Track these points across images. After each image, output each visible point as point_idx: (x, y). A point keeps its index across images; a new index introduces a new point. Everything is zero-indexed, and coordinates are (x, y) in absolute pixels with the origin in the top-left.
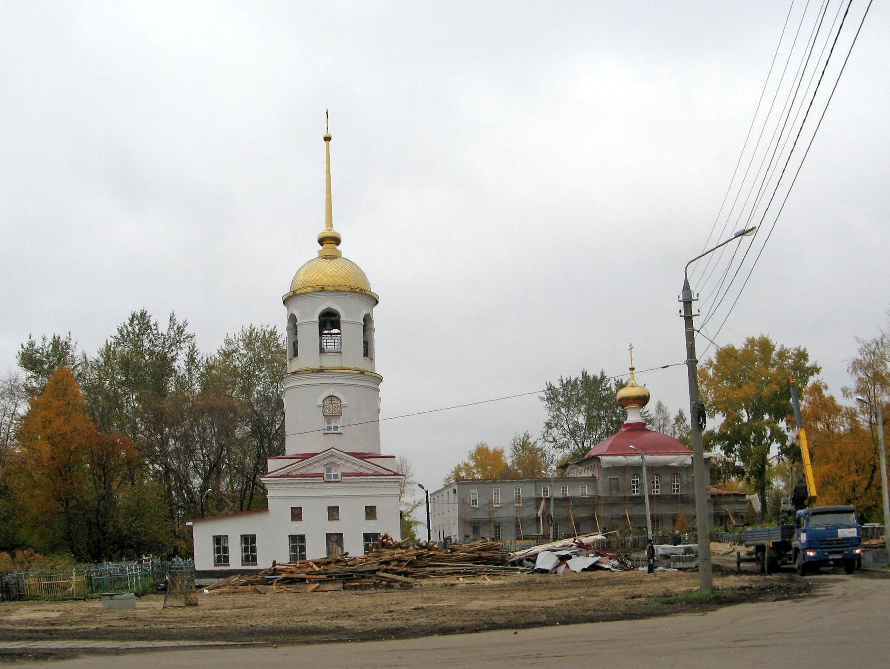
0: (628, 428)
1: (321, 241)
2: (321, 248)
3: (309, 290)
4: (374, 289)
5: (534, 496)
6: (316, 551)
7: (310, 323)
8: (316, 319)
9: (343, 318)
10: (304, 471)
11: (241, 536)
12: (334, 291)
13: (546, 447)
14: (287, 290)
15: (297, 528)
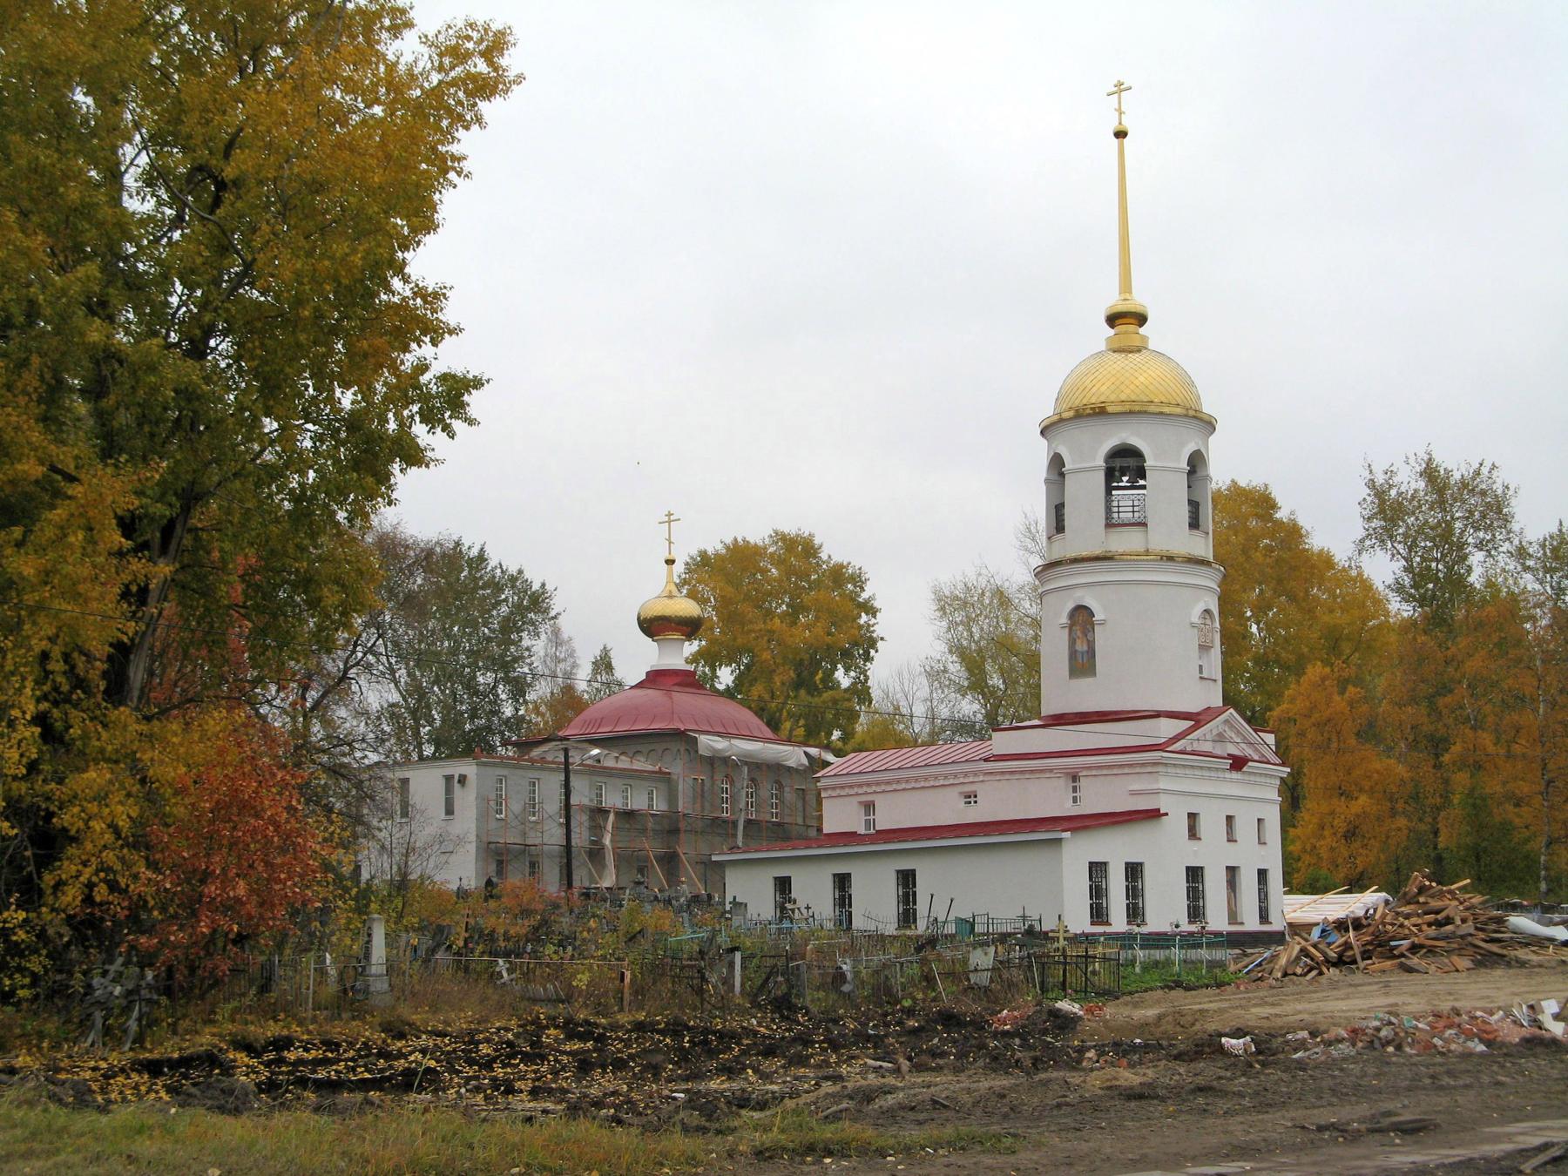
0: (678, 680)
1: (1113, 319)
2: (1112, 332)
3: (1178, 410)
4: (1208, 408)
8: (1100, 462)
9: (1149, 463)
10: (1189, 749)
11: (1188, 868)
12: (1186, 416)
13: (75, 732)
14: (1047, 411)
15: (1194, 854)
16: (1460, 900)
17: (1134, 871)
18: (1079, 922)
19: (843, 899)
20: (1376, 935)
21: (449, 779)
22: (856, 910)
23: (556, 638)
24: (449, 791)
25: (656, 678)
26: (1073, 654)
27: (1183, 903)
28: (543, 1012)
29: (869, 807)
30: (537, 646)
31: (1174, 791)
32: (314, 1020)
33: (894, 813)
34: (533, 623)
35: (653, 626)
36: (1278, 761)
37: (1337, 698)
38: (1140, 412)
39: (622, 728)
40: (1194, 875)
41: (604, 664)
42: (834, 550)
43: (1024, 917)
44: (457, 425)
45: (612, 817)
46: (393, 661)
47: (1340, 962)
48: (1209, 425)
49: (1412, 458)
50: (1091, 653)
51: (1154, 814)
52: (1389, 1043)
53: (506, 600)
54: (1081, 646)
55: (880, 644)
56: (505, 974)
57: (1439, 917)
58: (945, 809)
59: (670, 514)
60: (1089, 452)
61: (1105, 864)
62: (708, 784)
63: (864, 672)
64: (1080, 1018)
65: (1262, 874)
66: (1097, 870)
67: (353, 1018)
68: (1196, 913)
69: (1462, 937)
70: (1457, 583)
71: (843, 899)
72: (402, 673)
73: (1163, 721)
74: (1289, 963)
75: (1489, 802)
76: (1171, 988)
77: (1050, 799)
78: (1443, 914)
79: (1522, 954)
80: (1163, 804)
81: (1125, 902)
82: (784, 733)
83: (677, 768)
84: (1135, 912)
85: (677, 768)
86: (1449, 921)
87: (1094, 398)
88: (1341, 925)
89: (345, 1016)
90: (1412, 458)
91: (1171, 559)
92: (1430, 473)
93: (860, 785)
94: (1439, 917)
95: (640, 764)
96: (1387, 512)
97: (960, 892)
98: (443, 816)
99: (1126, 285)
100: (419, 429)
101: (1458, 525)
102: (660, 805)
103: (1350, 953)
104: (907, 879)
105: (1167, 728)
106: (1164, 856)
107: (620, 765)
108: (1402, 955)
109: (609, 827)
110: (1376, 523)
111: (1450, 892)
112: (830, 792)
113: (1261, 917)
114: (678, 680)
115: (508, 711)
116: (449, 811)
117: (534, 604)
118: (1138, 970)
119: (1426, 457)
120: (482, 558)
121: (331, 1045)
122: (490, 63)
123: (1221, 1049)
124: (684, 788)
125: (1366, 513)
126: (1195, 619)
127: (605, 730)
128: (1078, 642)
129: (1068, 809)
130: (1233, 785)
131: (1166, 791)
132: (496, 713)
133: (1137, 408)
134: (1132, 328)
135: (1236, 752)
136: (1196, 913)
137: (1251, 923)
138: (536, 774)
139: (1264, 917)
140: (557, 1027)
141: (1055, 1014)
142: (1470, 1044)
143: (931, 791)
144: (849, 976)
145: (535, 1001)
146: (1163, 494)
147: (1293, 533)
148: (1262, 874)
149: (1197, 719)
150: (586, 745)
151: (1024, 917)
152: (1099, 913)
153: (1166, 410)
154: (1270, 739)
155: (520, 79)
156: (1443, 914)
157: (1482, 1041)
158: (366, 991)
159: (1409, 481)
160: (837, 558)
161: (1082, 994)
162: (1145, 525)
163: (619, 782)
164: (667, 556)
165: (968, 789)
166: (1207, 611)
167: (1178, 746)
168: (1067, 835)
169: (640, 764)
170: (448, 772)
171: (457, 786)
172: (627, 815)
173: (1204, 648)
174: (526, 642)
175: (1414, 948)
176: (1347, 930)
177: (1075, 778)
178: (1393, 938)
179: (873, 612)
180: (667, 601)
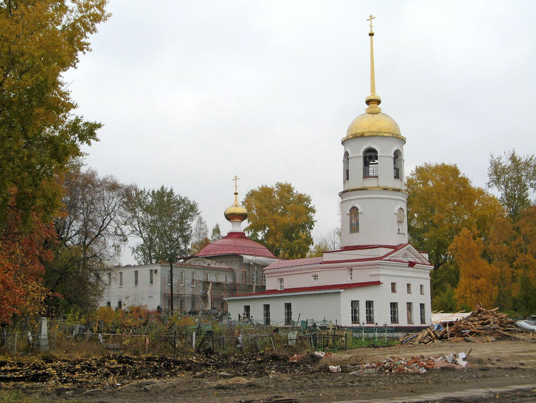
1: (368, 102)
2: (368, 107)
3: (390, 135)
4: (403, 134)
5: (202, 279)
6: (382, 318)
7: (388, 157)
8: (361, 154)
9: (379, 154)
10: (392, 259)
11: (367, 301)
14: (344, 135)
16: (493, 317)
17: (369, 304)
18: (346, 321)
19: (267, 314)
20: (456, 328)
21: (151, 271)
22: (272, 317)
23: (200, 221)
24: (151, 275)
25: (231, 235)
26: (351, 225)
27: (389, 316)
28: (112, 353)
29: (281, 280)
30: (193, 224)
31: (386, 274)
32: (16, 355)
33: (290, 283)
34: (191, 216)
35: (230, 217)
36: (429, 264)
37: (472, 242)
38: (375, 136)
39: (217, 253)
40: (394, 305)
41: (217, 230)
42: (299, 189)
43: (325, 321)
44: (92, 141)
45: (211, 284)
46: (142, 229)
47: (441, 338)
48: (403, 141)
49: (507, 152)
50: (357, 224)
51: (378, 283)
52: (387, 368)
53: (181, 208)
54: (354, 222)
55: (315, 223)
56: (101, 339)
57: (485, 322)
58: (307, 281)
59: (236, 177)
60: (358, 150)
61: (358, 301)
62: (247, 273)
63: (309, 233)
64: (321, 358)
65: (422, 306)
66: (355, 304)
67: (33, 355)
68: (394, 319)
69: (494, 329)
70: (523, 200)
71: (267, 314)
72: (145, 235)
73: (382, 249)
74: (422, 338)
75: (531, 280)
76: (370, 347)
77: (342, 278)
78: (487, 321)
79: (518, 336)
80: (381, 279)
81: (366, 315)
82: (281, 255)
83: (235, 267)
84: (370, 319)
85: (235, 267)
86: (489, 323)
87: (360, 131)
88: (445, 324)
89: (29, 354)
90: (507, 152)
91: (386, 189)
92: (513, 158)
93: (278, 273)
94: (485, 322)
95: (223, 266)
96: (497, 172)
97: (307, 311)
98: (149, 284)
99: (373, 90)
100: (78, 142)
101: (523, 178)
102: (230, 281)
103: (446, 335)
104: (288, 306)
105: (383, 252)
106: (382, 299)
107: (217, 266)
108: (466, 336)
109: (210, 288)
110: (493, 177)
111: (491, 312)
112: (268, 275)
113: (421, 321)
114: (239, 236)
115: (183, 247)
116: (151, 282)
117: (191, 209)
118: (363, 340)
119: (512, 153)
120: (171, 192)
121: (20, 364)
122: (100, 9)
123: (328, 370)
124: (238, 274)
125: (490, 173)
126: (396, 212)
127: (212, 254)
128: (353, 220)
129: (349, 281)
130: (410, 272)
131: (382, 275)
132: (179, 248)
133: (374, 134)
134: (375, 105)
135: (412, 260)
136: (394, 319)
137: (417, 323)
138: (183, 269)
139: (423, 321)
140: (115, 359)
141: (313, 356)
142: (421, 369)
143: (302, 275)
144: (240, 341)
145: (110, 349)
146: (383, 166)
147: (465, 182)
148: (422, 306)
149: (396, 248)
150: (205, 259)
151: (325, 321)
152: (355, 319)
153: (385, 135)
154: (426, 256)
155: (110, 15)
156: (487, 321)
157: (425, 368)
158: (39, 345)
159: (506, 162)
160: (299, 192)
161: (323, 348)
162: (377, 177)
163: (214, 272)
164: (235, 192)
165: (315, 274)
166: (401, 208)
167: (387, 258)
168: (342, 290)
169: (223, 266)
170: (151, 268)
171: (154, 273)
172: (217, 284)
173: (400, 222)
174: (189, 223)
175: (471, 333)
176: (446, 326)
177: (351, 270)
178: (463, 329)
179: (314, 211)
180: (235, 207)
